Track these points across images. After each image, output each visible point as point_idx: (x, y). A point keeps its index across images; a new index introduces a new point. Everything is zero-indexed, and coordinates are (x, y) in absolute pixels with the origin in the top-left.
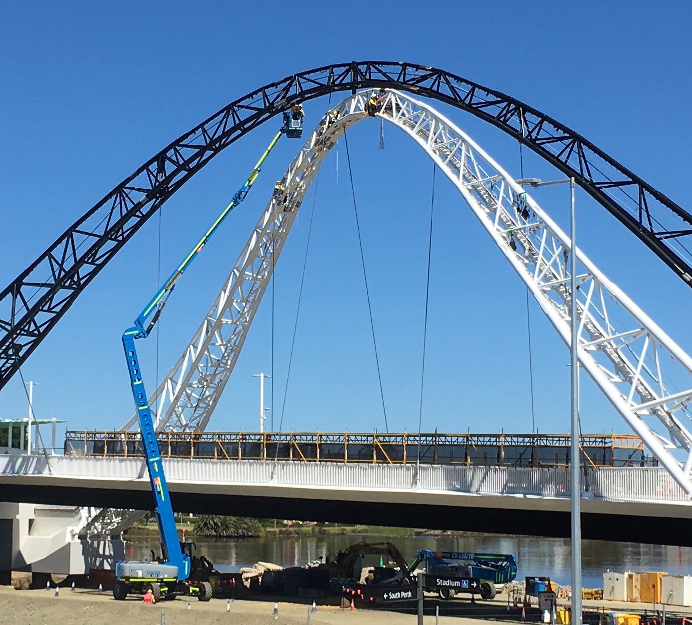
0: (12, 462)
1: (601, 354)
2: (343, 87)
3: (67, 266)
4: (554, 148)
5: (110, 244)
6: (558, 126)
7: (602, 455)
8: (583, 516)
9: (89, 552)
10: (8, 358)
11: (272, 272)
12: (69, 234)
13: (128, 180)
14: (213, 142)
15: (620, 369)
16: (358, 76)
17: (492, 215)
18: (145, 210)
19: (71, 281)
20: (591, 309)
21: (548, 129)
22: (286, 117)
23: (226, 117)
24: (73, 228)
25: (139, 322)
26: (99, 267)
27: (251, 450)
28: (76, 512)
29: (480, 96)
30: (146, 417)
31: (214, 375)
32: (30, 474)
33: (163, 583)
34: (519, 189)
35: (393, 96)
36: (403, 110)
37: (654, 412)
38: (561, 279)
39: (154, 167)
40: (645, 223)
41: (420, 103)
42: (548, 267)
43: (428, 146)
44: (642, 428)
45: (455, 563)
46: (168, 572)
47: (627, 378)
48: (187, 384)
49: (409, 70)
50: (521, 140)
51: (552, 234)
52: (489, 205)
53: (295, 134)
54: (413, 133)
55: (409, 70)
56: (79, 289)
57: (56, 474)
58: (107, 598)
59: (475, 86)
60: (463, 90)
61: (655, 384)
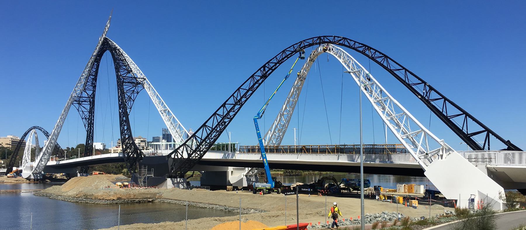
0: (225, 154)
1: (392, 120)
2: (316, 44)
3: (238, 99)
4: (379, 60)
5: (250, 92)
6: (380, 53)
7: (394, 150)
8: (364, 167)
9: (248, 180)
10: (222, 125)
11: (298, 99)
12: (238, 89)
13: (255, 73)
14: (279, 61)
15: (398, 125)
16: (321, 40)
17: (359, 81)
18: (260, 82)
19: (240, 103)
20: (389, 107)
21: (378, 54)
22: (300, 53)
23: (283, 54)
24: (240, 88)
25: (258, 114)
26: (247, 99)
27: (291, 150)
28: (244, 169)
29: (357, 45)
30: (261, 142)
31: (282, 129)
32: (230, 158)
33: (267, 189)
34: (367, 72)
35: (331, 46)
36: (334, 50)
37: (408, 137)
38: (380, 99)
39: (262, 69)
40: (407, 81)
41: (339, 48)
42: (376, 95)
43: (341, 60)
44: (403, 142)
45: (353, 182)
46: (268, 186)
47: (399, 127)
48: (274, 132)
49: (336, 38)
50: (370, 58)
51: (377, 85)
52: (359, 78)
53: (303, 58)
54: (336, 57)
55: (336, 38)
56: (242, 105)
57: (237, 158)
58: (251, 193)
59: (355, 42)
60: (352, 43)
61: (408, 129)
